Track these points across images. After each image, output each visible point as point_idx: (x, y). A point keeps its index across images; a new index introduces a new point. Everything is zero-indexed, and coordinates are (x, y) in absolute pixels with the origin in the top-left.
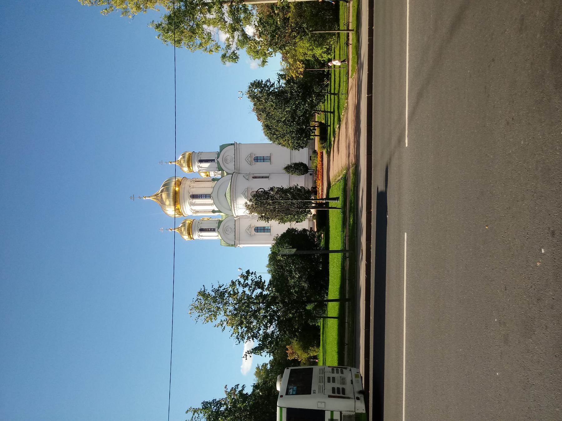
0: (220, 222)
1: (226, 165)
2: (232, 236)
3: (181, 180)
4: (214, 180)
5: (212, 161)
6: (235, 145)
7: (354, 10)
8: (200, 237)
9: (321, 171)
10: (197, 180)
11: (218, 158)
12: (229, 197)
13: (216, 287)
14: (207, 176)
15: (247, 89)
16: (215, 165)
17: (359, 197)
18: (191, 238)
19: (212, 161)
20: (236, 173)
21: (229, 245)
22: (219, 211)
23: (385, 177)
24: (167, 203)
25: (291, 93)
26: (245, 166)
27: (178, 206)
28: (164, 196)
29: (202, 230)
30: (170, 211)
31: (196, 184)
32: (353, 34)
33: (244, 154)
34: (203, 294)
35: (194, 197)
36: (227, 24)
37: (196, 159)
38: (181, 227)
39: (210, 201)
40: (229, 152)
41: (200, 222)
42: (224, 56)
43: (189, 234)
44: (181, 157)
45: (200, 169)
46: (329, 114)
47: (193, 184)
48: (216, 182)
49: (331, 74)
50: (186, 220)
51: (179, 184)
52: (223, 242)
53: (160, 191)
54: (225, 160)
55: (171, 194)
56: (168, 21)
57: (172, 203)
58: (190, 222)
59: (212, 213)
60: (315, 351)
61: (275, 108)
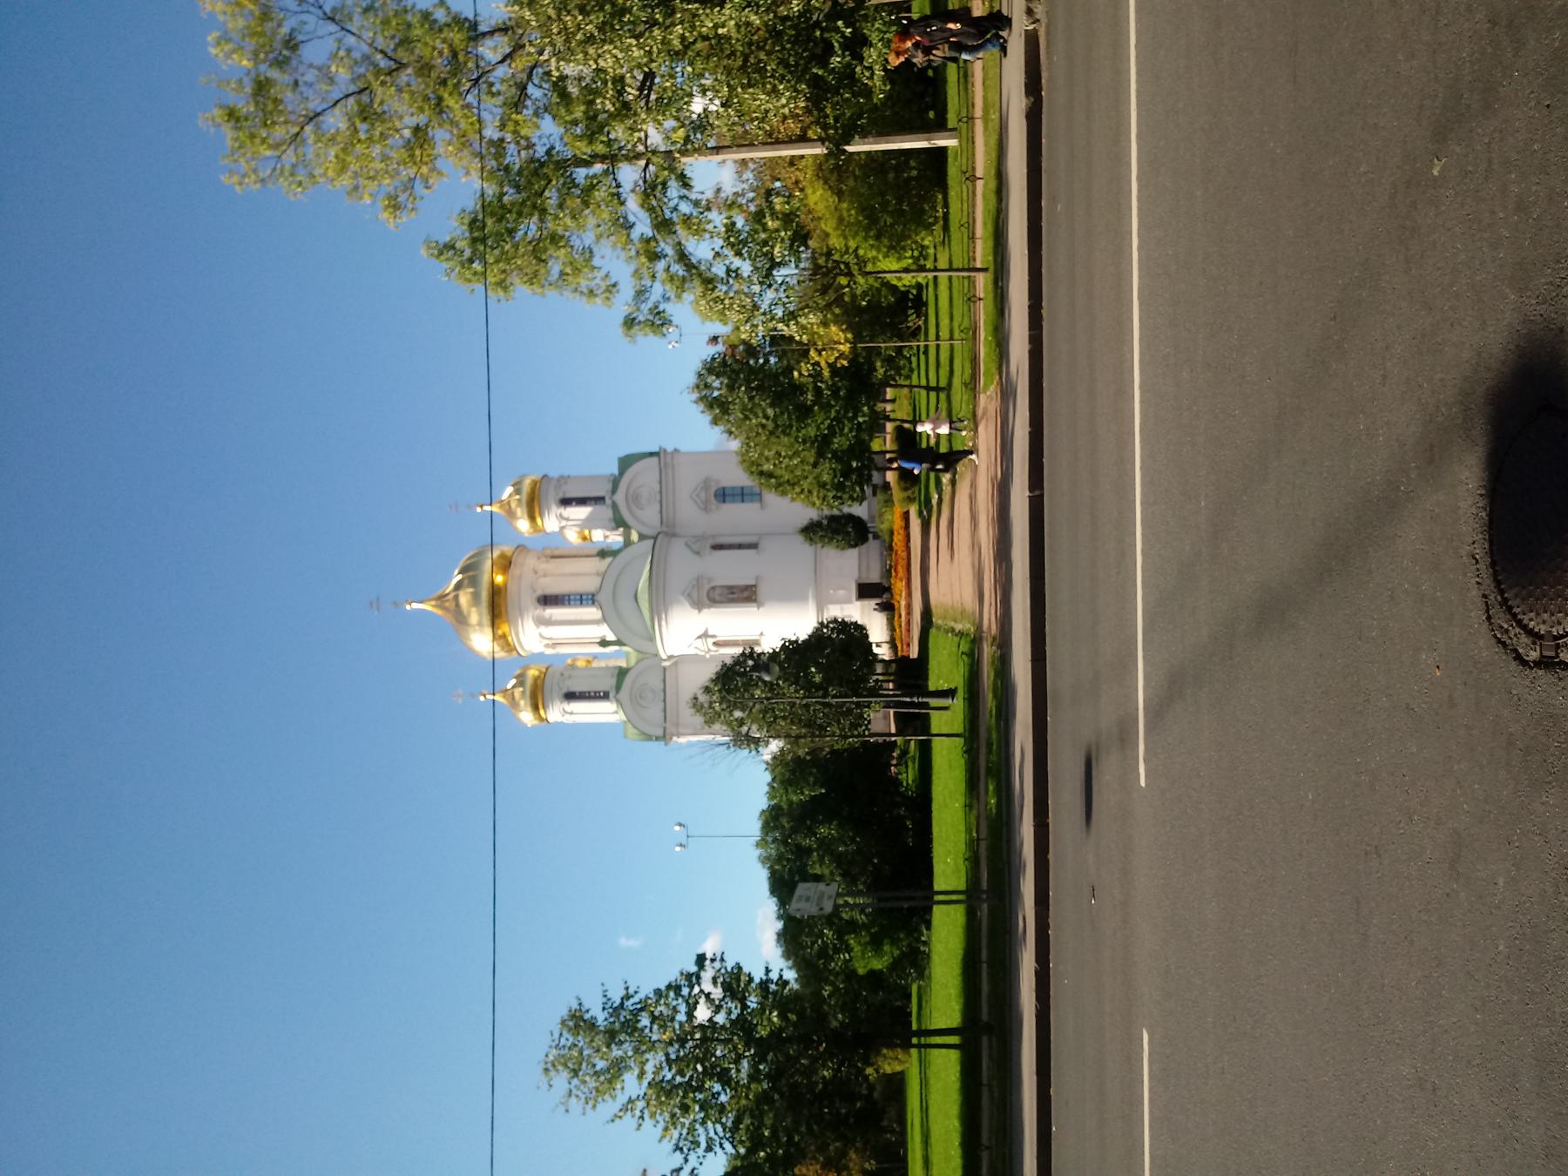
0: (622, 673)
1: (638, 512)
2: (655, 712)
3: (509, 554)
4: (603, 554)
5: (599, 500)
6: (662, 455)
7: (987, 153)
8: (567, 716)
9: (904, 555)
10: (556, 553)
11: (614, 491)
12: (646, 596)
13: (616, 996)
14: (585, 539)
15: (692, 379)
16: (605, 512)
17: (1014, 755)
18: (541, 719)
19: (599, 500)
20: (666, 534)
21: (649, 738)
22: (619, 643)
23: (1083, 775)
24: (474, 618)
25: (818, 391)
26: (688, 513)
27: (504, 628)
28: (464, 599)
29: (571, 696)
30: (481, 641)
31: (554, 566)
32: (985, 278)
33: (687, 482)
34: (578, 1021)
35: (548, 600)
36: (636, 234)
37: (552, 496)
38: (514, 687)
39: (592, 612)
40: (645, 476)
41: (566, 674)
42: (630, 322)
43: (536, 708)
44: (510, 490)
45: (564, 523)
46: (924, 393)
47: (544, 566)
48: (609, 560)
49: (926, 304)
50: (526, 668)
51: (506, 564)
52: (631, 731)
53: (451, 587)
54: (634, 499)
55: (485, 595)
56: (471, 233)
57: (486, 619)
58: (537, 673)
59: (597, 646)
60: (897, 1058)
61: (772, 433)
